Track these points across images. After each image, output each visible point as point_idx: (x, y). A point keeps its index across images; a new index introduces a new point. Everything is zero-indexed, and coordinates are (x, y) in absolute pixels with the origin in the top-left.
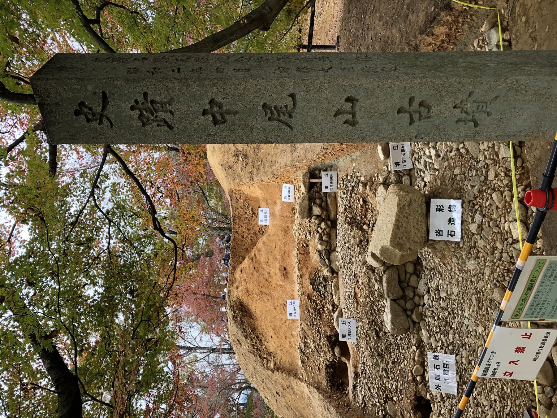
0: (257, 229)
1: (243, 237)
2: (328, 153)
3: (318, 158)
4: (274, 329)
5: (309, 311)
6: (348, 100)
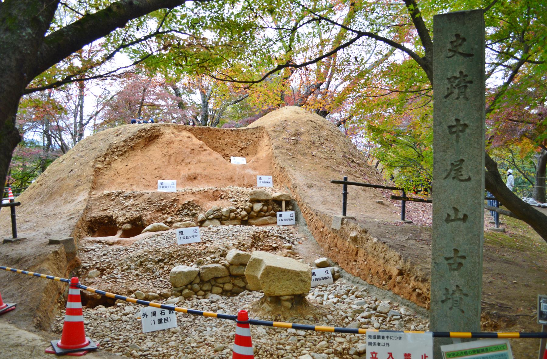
0: (227, 152)
1: (220, 139)
2: (312, 217)
3: (305, 208)
4: (135, 168)
5: (162, 200)
6: (465, 216)
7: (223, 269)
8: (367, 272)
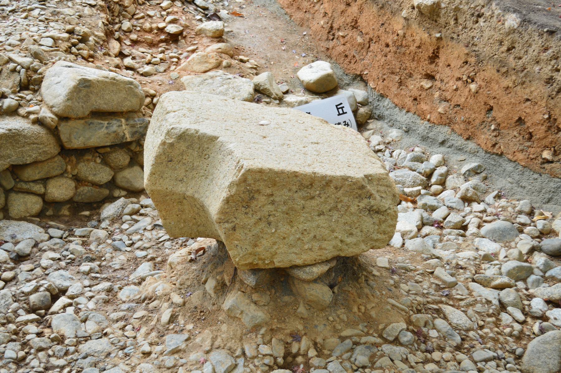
7: (38, 136)
8: (478, 116)
